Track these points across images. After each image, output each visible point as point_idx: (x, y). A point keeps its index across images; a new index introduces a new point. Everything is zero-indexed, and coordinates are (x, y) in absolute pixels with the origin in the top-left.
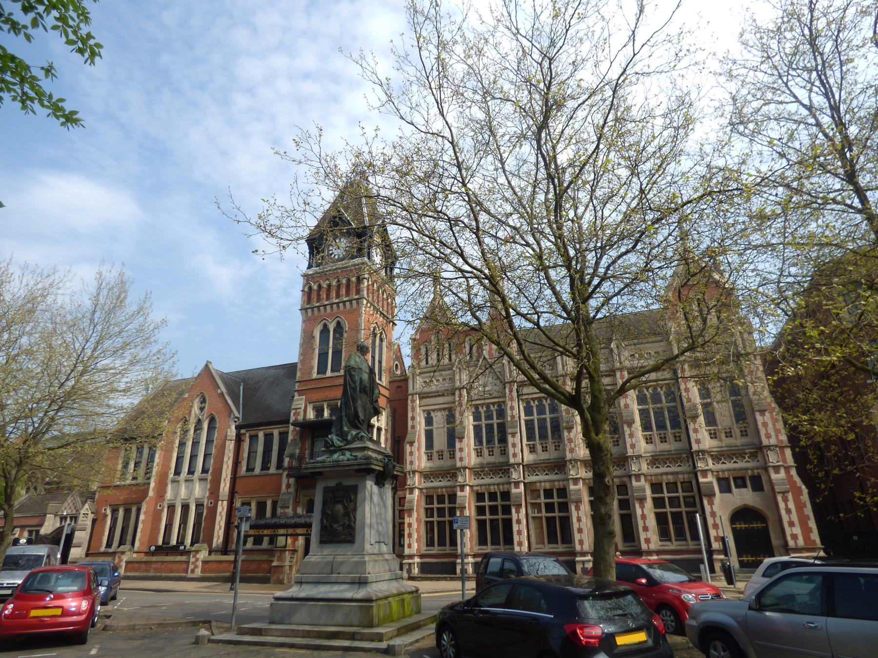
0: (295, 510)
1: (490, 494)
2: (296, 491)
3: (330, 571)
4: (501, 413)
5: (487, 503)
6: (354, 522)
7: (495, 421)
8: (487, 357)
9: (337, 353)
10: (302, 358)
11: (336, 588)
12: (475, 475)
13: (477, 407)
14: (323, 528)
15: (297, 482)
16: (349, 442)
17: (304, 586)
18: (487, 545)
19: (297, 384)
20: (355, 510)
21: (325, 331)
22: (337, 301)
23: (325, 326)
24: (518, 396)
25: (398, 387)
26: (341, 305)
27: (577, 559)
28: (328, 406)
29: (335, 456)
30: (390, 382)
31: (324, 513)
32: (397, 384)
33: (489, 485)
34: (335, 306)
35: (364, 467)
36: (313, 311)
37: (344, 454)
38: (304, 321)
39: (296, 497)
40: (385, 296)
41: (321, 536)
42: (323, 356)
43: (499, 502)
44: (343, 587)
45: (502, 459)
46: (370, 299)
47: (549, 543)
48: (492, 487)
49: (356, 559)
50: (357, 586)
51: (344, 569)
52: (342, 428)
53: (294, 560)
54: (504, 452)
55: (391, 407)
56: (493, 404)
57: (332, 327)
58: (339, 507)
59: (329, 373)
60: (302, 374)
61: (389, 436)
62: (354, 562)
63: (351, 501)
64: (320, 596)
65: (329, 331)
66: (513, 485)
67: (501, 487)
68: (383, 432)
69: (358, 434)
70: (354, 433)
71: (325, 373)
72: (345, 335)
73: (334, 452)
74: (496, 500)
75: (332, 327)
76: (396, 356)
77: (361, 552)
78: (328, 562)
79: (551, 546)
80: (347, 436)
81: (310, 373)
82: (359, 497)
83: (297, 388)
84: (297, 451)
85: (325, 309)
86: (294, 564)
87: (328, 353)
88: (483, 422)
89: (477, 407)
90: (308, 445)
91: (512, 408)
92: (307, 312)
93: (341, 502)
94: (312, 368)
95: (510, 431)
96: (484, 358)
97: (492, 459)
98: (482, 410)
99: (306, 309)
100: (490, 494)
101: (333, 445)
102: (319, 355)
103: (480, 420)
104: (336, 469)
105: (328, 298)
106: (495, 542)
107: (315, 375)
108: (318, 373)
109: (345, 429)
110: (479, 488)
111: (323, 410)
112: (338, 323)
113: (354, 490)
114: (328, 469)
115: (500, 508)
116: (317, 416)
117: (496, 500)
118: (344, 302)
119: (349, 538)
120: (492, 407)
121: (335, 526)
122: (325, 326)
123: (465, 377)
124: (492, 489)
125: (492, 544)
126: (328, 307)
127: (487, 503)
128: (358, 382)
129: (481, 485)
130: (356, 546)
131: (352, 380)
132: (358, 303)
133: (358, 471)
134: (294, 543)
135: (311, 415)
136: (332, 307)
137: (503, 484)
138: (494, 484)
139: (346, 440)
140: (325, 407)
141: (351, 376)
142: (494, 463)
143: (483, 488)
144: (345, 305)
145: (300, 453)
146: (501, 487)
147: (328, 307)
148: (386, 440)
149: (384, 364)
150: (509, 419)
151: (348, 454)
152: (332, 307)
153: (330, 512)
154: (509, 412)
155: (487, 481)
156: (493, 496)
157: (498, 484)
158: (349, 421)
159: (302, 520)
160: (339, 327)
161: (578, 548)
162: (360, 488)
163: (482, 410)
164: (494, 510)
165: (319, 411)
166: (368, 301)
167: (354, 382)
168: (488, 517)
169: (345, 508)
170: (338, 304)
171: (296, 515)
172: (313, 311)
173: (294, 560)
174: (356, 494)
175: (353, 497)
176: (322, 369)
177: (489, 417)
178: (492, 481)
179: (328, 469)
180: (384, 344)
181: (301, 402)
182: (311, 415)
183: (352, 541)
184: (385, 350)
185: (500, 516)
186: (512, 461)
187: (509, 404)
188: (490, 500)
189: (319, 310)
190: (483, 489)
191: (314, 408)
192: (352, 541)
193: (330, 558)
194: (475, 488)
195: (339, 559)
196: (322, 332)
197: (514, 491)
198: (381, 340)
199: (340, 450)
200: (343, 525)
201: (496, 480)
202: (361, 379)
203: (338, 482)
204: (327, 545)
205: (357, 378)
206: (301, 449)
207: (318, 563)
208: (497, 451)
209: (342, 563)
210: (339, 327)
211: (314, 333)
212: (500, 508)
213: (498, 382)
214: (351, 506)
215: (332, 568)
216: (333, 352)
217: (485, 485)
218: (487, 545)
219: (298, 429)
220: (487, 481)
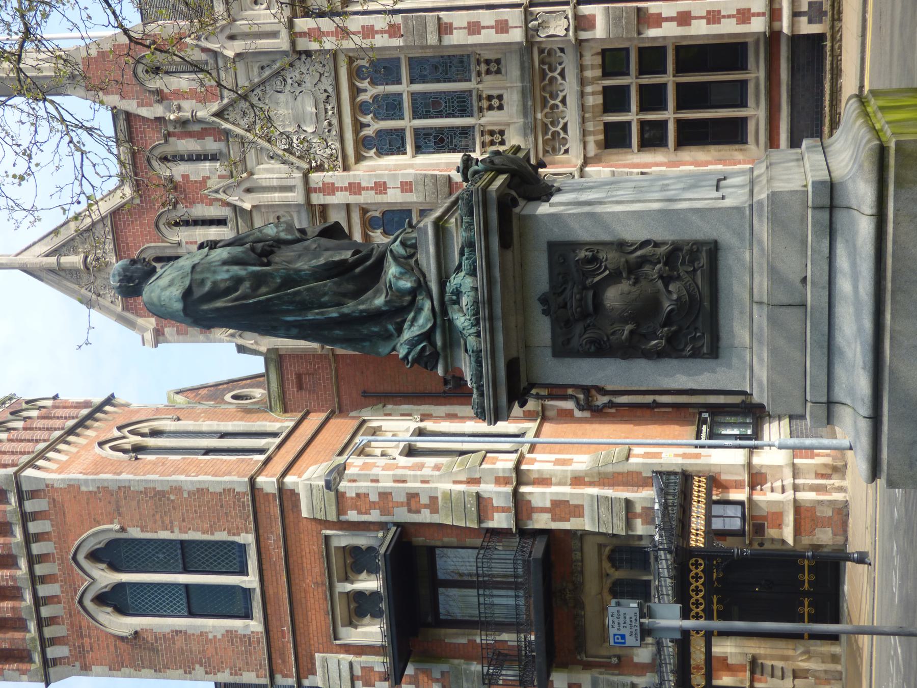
0: (641, 669)
1: (608, 108)
2: (587, 666)
3: (798, 311)
4: (384, 68)
5: (633, 116)
6: (657, 245)
7: (405, 88)
8: (215, 107)
9: (187, 555)
10: (199, 670)
11: (844, 285)
12: (555, 151)
13: (363, 144)
14: (672, 349)
15: (564, 665)
16: (421, 286)
17: (840, 393)
18: (744, 120)
19: (280, 680)
20: (621, 245)
21: (117, 600)
22: (23, 563)
23: (102, 599)
24: (332, 14)
25: (300, 387)
26: (36, 549)
27: (786, 30)
28: (347, 579)
29: (461, 320)
30: (285, 411)
31: (630, 350)
32: (292, 389)
33: (583, 108)
34: (39, 570)
35: (494, 215)
36: (54, 641)
37: (458, 293)
38: (85, 669)
39: (606, 666)
40: (20, 424)
41: (696, 354)
42: (197, 602)
43: (632, 81)
44: (843, 262)
45: (513, 70)
46: (25, 459)
47: (744, 67)
48: (591, 101)
49: (763, 229)
50: (841, 216)
51: (791, 266)
52: (376, 316)
53: (779, 664)
54: (493, 65)
55: (359, 406)
56: (355, 91)
57: (106, 578)
58: (614, 296)
59: (250, 581)
60: (248, 666)
61: (442, 410)
62: (773, 233)
63: (594, 259)
64: (868, 324)
65: (120, 587)
66: (584, 35)
67: (589, 74)
68: (429, 425)
69: (396, 258)
70: (392, 270)
71: (247, 593)
72: (135, 533)
73: (449, 327)
74: (624, 91)
75: (106, 578)
76: (209, 398)
77: (742, 217)
78: (773, 321)
79: (751, 101)
80: (402, 293)
81: (247, 639)
82: (583, 234)
83: (292, 681)
84: (476, 667)
85: (48, 600)
86: (788, 666)
87: (187, 587)
88: (408, 123)
89: (363, 144)
90: (460, 638)
91: (368, 32)
92: (55, 662)
93: (598, 291)
94: (230, 634)
95: (432, 39)
96: (219, 114)
97: (513, 100)
98: (374, 126)
99: (47, 663)
100: (608, 108)
101: (428, 336)
102: (191, 614)
103: (399, 134)
104: (498, 310)
105: (18, 624)
106: (737, 95)
107: (255, 625)
108: (248, 616)
109: (379, 301)
110: (591, 139)
111: (359, 595)
112: (95, 556)
113: (561, 251)
114: (500, 338)
115: (647, 80)
116: (377, 614)
117: (624, 91)
118: (29, 539)
119: (704, 260)
120: (364, 97)
121: (667, 306)
122: (102, 599)
123: (268, 172)
124: (595, 100)
125: (743, 104)
126: (44, 590)
127: (633, 116)
128: (237, 270)
129: (584, 133)
130: (726, 237)
131: (227, 292)
132: (34, 494)
133: (506, 243)
134: (730, 669)
135: (372, 632)
136: (44, 579)
137: (582, 68)
138: (582, 95)
139: (413, 292)
140: (349, 587)
141: (215, 294)
142: (523, 93)
143: (590, 126)
144: (38, 537)
145: (481, 660)
146: (589, 74)
147: (44, 590)
148: (452, 417)
149: (230, 426)
150: (398, 42)
151: (456, 280)
152: (44, 579)
153: (628, 328)
154: (380, 41)
155: (571, 115)
156: (614, 100)
157: (582, 82)
158: (356, 295)
159: (670, 649)
160: (113, 554)
161: (758, 25)
162: (558, 234)
163: (374, 126)
164: (652, 98)
165: (361, 606)
166: (30, 464)
167: (237, 281)
168: (669, 115)
169: (615, 277)
170: (32, 561)
171: (655, 666)
172: (54, 641)
173: (779, 664)
174: (575, 245)
175: (582, 254)
176: (233, 603)
177: (390, 107)
178: (572, 101)
179: (500, 338)
180: (168, 425)
181: (333, 667)
182: (372, 632)
183: (713, 249)
184: (187, 425)
185: (669, 79)
186: (516, 35)
187: (357, 41)
188: (626, 109)
189: (52, 621)
190: (595, 127)
191: (351, 624)
192: (713, 249)
193: (760, 317)
194: (592, 150)
195: (762, 284)
196: (122, 610)
197: (600, 31)
198: (155, 433)
199: (442, 315)
200: (667, 280)
201: (569, 87)
202: (225, 263)
203: (537, 309)
204: (724, 334)
205: (223, 275)
206: (469, 658)
207: (774, 352)
208: (489, 85)
209: (774, 273)
210: (113, 554)
211: (126, 632)
212: (647, 80)
213: (292, 75)
214: (611, 258)
215: (788, 304)
216: (186, 570)
217: (583, 120)
218: (744, 120)
219: (410, 670)
220: (571, 115)
